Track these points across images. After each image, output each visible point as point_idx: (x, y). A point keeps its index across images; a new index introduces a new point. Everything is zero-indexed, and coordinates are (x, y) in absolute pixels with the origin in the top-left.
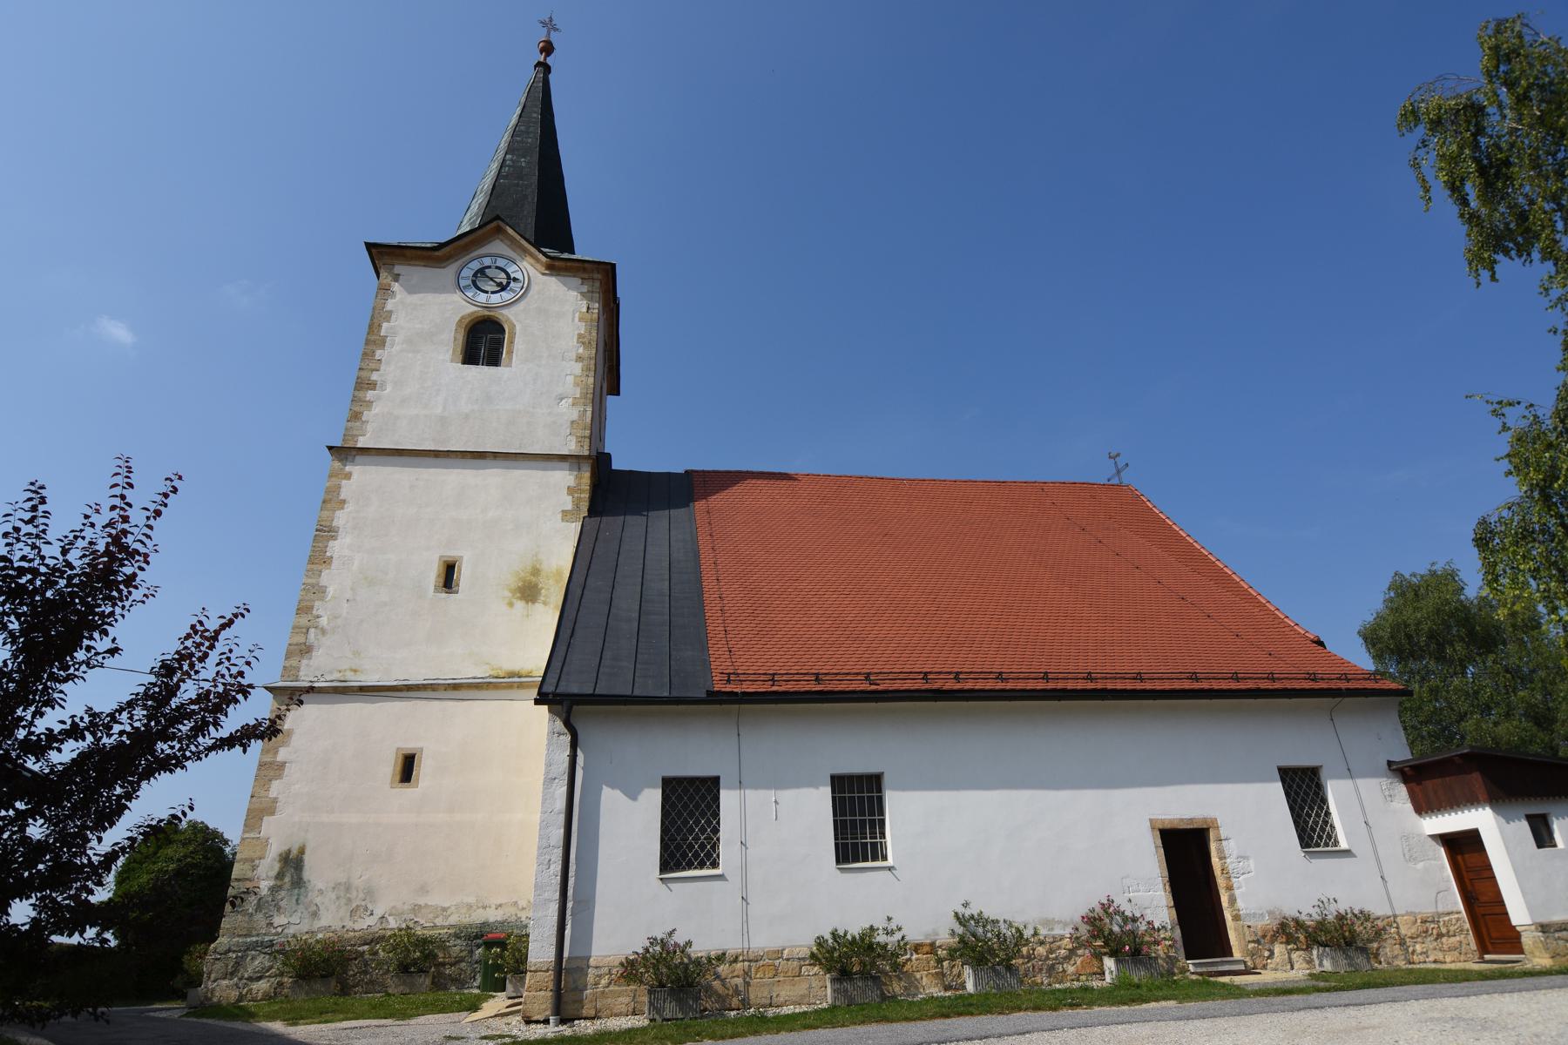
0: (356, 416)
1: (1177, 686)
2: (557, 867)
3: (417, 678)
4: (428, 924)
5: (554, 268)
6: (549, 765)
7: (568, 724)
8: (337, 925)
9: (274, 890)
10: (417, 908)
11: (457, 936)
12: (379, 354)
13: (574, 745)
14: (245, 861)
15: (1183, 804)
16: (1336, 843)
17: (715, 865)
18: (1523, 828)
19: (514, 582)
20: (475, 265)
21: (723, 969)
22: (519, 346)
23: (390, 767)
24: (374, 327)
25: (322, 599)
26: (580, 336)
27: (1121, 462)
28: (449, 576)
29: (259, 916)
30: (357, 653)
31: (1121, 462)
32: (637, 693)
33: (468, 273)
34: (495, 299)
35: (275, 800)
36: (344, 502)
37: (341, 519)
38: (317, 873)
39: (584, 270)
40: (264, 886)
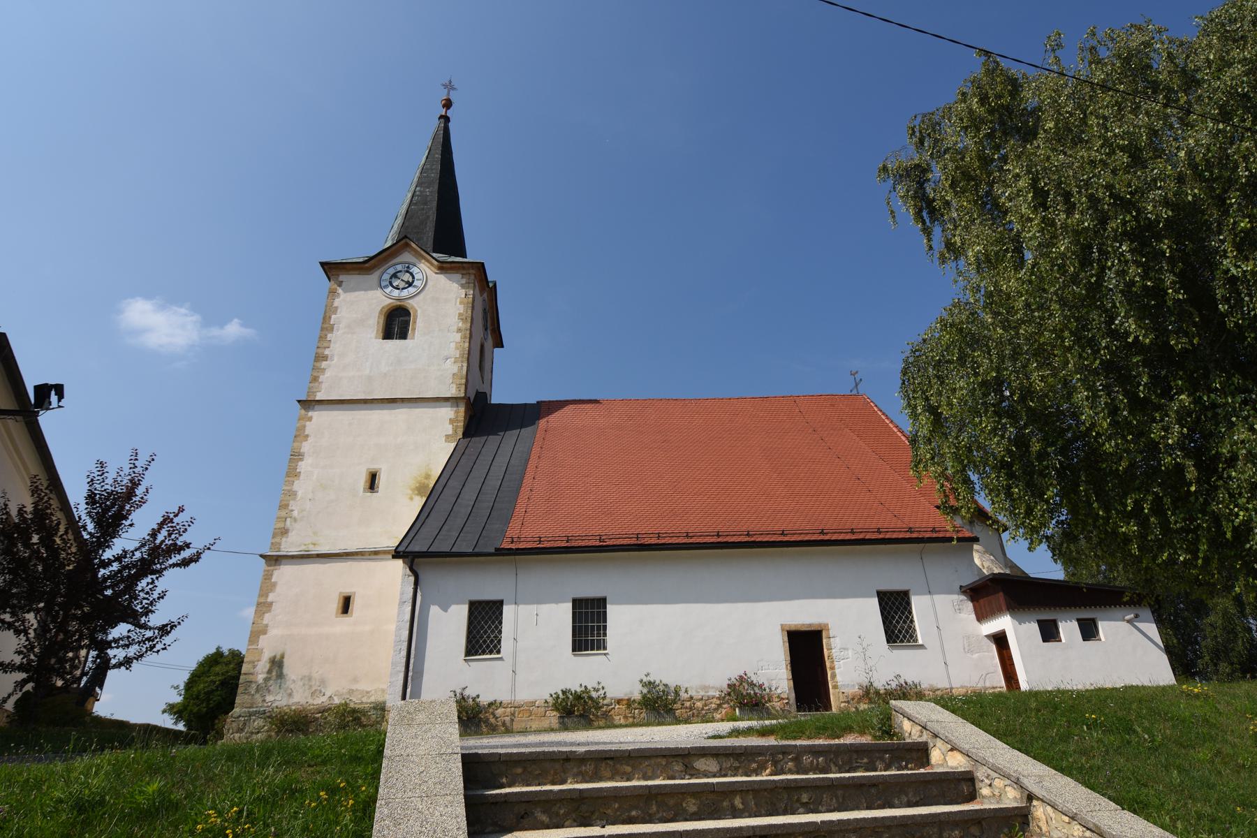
0: (315, 379)
1: (841, 537)
2: (404, 653)
3: (352, 548)
4: (356, 701)
5: (443, 268)
6: (402, 594)
7: (411, 569)
8: (303, 702)
9: (266, 680)
10: (351, 692)
11: (374, 708)
12: (329, 336)
13: (416, 583)
14: (249, 662)
15: (804, 613)
16: (916, 640)
17: (499, 652)
18: (1033, 628)
19: (413, 484)
20: (391, 271)
21: (500, 711)
22: (419, 325)
23: (336, 604)
24: (326, 319)
25: (294, 499)
26: (460, 314)
27: (858, 377)
28: (373, 481)
29: (257, 696)
30: (315, 533)
31: (858, 377)
33: (386, 277)
34: (405, 293)
35: (267, 626)
36: (307, 436)
37: (306, 447)
38: (291, 670)
39: (464, 268)
40: (260, 678)
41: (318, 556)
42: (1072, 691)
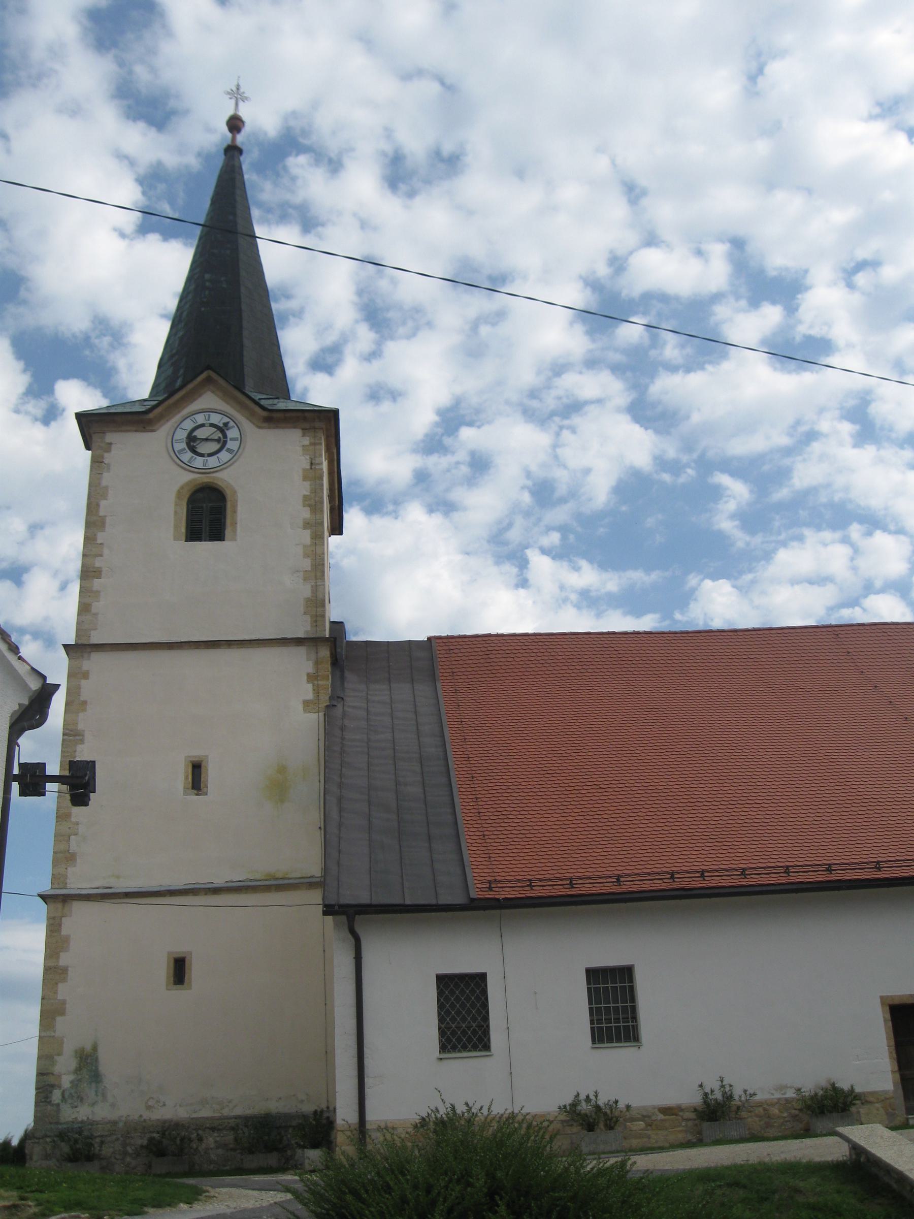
9: (75, 1084)
20: (188, 425)
22: (243, 515)
32: (408, 902)
34: (212, 462)
35: (64, 1002)
36: (85, 703)
40: (66, 1081)
41: (127, 895)
42: (235, 215)
